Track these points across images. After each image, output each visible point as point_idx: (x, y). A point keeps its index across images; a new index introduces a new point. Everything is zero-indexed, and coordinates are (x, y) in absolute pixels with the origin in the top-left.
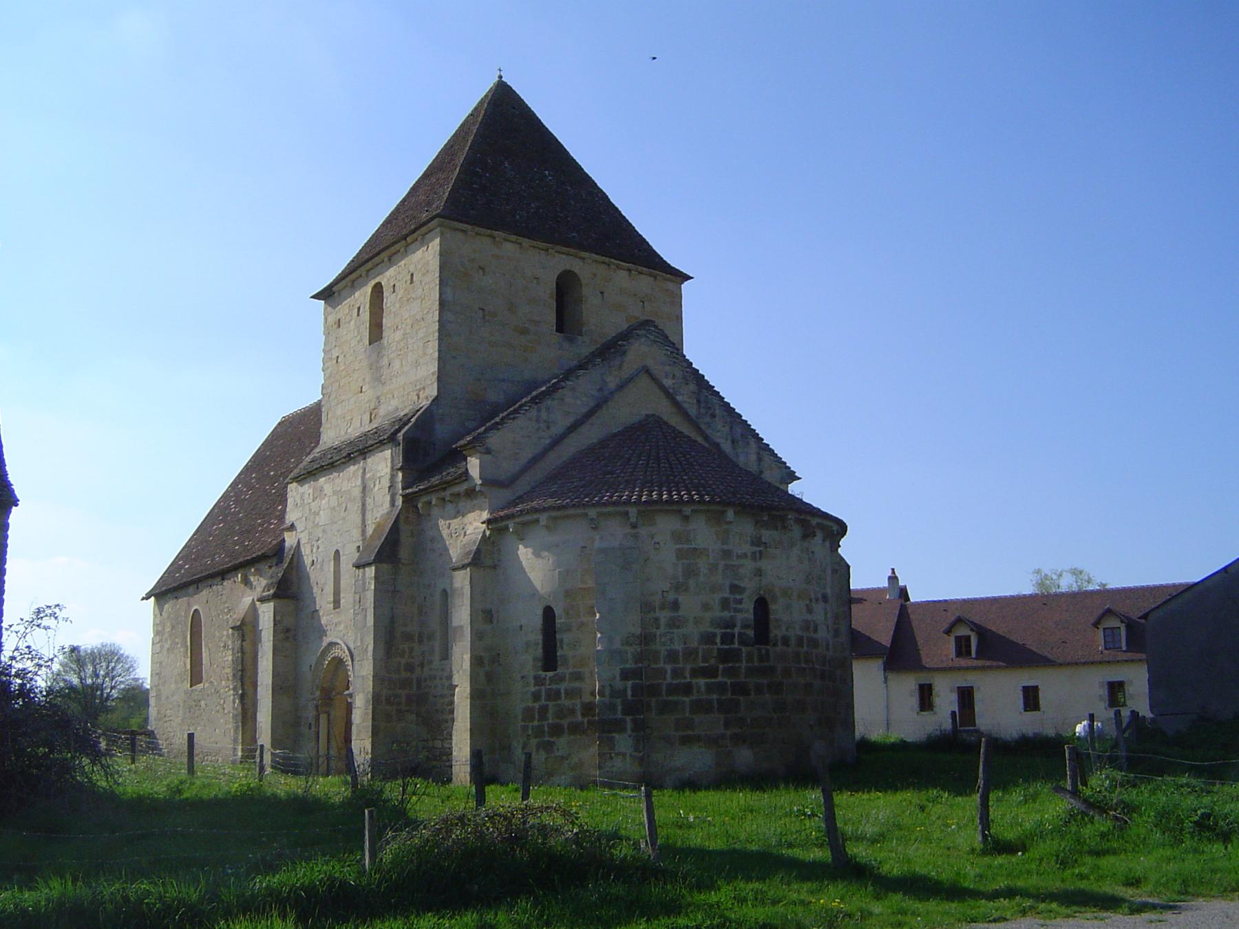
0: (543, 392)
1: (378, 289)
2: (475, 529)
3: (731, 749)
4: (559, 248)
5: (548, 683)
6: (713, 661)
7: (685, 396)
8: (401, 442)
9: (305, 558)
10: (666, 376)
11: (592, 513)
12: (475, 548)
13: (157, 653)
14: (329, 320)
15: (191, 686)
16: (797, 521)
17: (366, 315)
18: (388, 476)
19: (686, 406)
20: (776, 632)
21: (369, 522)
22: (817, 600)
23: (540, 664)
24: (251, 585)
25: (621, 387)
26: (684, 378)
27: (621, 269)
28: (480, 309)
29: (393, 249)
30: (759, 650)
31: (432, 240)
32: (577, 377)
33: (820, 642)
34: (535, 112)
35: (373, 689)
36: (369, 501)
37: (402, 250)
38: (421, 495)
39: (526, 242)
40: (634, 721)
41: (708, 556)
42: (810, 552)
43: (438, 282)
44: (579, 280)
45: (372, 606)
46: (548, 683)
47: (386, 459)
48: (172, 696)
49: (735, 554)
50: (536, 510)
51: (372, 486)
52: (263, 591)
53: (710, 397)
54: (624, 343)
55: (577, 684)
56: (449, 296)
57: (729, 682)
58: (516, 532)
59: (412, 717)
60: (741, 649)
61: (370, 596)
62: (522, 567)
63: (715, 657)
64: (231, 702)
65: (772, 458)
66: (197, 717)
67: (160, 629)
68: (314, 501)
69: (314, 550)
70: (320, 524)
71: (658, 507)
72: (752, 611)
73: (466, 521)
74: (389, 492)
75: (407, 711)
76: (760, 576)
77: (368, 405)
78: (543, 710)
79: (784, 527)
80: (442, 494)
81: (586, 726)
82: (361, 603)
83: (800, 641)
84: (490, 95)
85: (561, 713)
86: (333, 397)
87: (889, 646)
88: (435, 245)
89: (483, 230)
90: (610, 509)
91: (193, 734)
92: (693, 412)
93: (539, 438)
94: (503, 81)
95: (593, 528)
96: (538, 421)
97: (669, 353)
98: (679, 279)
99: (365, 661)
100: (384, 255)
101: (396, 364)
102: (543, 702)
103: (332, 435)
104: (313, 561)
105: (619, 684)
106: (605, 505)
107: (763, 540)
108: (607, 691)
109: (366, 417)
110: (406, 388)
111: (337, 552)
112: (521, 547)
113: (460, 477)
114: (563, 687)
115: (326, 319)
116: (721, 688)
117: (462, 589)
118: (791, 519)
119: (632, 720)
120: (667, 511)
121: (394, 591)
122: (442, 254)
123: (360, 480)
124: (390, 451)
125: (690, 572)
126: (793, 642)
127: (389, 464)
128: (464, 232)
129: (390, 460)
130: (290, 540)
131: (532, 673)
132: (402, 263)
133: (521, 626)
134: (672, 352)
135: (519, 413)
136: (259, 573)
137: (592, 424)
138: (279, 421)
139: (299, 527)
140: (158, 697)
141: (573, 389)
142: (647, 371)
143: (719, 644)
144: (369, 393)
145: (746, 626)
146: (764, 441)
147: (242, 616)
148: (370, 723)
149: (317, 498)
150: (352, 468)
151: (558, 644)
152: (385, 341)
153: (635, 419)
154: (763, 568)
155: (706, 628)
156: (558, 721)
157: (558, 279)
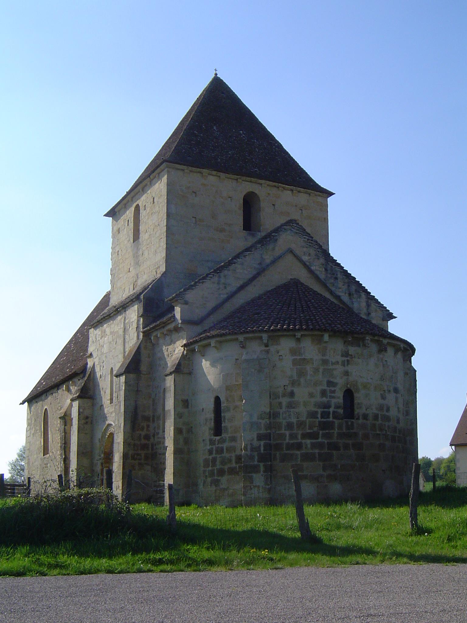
0: (222, 266)
1: (137, 207)
2: (179, 351)
3: (327, 484)
4: (244, 178)
5: (217, 443)
6: (315, 429)
7: (317, 267)
8: (142, 299)
9: (97, 373)
10: (305, 254)
11: (241, 338)
12: (178, 362)
13: (29, 437)
17: (132, 225)
18: (136, 321)
19: (318, 273)
23: (212, 432)
24: (71, 391)
25: (274, 262)
27: (286, 190)
30: (347, 422)
32: (245, 256)
33: (391, 417)
35: (123, 450)
36: (127, 337)
37: (148, 183)
38: (153, 332)
39: (222, 175)
42: (384, 361)
45: (123, 399)
46: (217, 443)
47: (135, 311)
48: (35, 462)
50: (209, 337)
51: (128, 328)
53: (334, 267)
54: (276, 234)
57: (326, 441)
59: (149, 468)
63: (317, 426)
65: (377, 305)
66: (46, 474)
67: (30, 422)
69: (101, 369)
70: (104, 353)
74: (136, 331)
75: (146, 464)
76: (348, 375)
77: (132, 279)
78: (214, 460)
79: (364, 345)
81: (238, 470)
82: (118, 398)
83: (376, 417)
88: (165, 179)
90: (251, 335)
92: (322, 276)
93: (220, 294)
95: (241, 347)
96: (218, 283)
97: (306, 240)
98: (325, 195)
99: (120, 433)
102: (214, 455)
104: (101, 375)
105: (256, 443)
106: (247, 332)
110: (150, 268)
112: (203, 360)
113: (171, 319)
114: (225, 446)
115: (113, 229)
116: (321, 446)
118: (368, 340)
119: (264, 465)
121: (138, 391)
122: (168, 185)
123: (123, 324)
125: (301, 373)
126: (370, 417)
127: (136, 314)
128: (183, 170)
129: (137, 311)
130: (90, 363)
132: (149, 192)
134: (308, 239)
135: (207, 279)
138: (105, 294)
139: (95, 355)
141: (242, 264)
142: (291, 251)
143: (320, 418)
144: (133, 272)
147: (65, 411)
148: (121, 471)
149: (102, 337)
150: (119, 318)
152: (140, 240)
153: (284, 282)
154: (349, 371)
157: (244, 196)
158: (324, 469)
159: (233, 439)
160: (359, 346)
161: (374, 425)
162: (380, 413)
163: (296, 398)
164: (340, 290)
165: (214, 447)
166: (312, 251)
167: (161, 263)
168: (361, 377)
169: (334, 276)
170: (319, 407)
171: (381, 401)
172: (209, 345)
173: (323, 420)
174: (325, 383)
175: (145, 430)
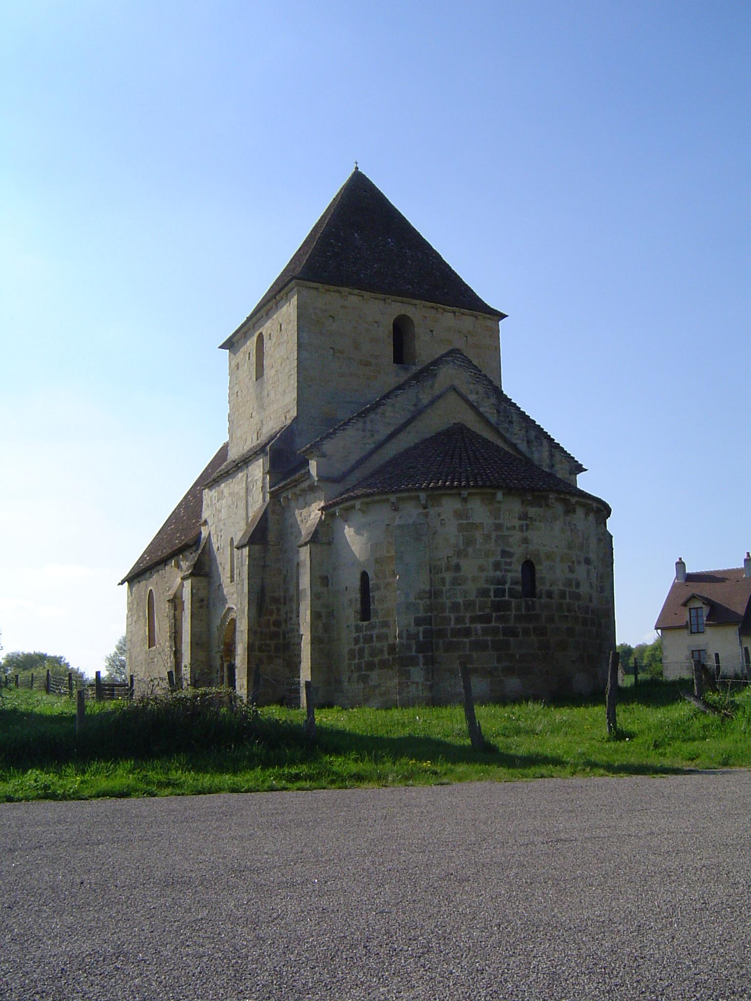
1: (261, 338)
3: (502, 678)
6: (488, 611)
7: (487, 408)
10: (471, 393)
11: (393, 498)
12: (314, 529)
14: (232, 364)
15: (149, 648)
16: (558, 499)
17: (254, 359)
18: (261, 479)
19: (488, 415)
20: (539, 588)
22: (579, 562)
24: (181, 568)
25: (432, 403)
26: (486, 393)
28: (330, 348)
30: (526, 602)
31: (292, 297)
32: (396, 396)
34: (384, 193)
36: (250, 499)
39: (367, 294)
43: (296, 329)
44: (412, 322)
49: (505, 527)
53: (508, 407)
54: (435, 368)
57: (501, 626)
58: (341, 516)
59: (279, 661)
60: (511, 602)
62: (347, 543)
65: (562, 454)
68: (218, 502)
69: (219, 539)
73: (311, 510)
78: (361, 651)
79: (547, 505)
83: (563, 595)
86: (235, 422)
87: (743, 615)
88: (294, 300)
89: (332, 288)
90: (405, 495)
92: (493, 420)
94: (358, 172)
95: (394, 510)
96: (364, 430)
98: (496, 318)
102: (362, 645)
105: (413, 629)
106: (401, 491)
107: (530, 516)
108: (405, 635)
109: (255, 437)
111: (232, 539)
112: (346, 527)
114: (375, 632)
115: (230, 364)
118: (552, 499)
119: (423, 657)
121: (264, 566)
124: (262, 460)
125: (469, 542)
127: (262, 470)
128: (317, 289)
130: (204, 534)
131: (354, 623)
132: (275, 317)
136: (186, 559)
137: (409, 432)
139: (210, 522)
141: (393, 406)
142: (454, 389)
144: (256, 418)
145: (516, 583)
146: (555, 441)
150: (240, 475)
151: (371, 599)
152: (265, 377)
155: (482, 584)
158: (499, 660)
168: (544, 546)
172: (353, 507)
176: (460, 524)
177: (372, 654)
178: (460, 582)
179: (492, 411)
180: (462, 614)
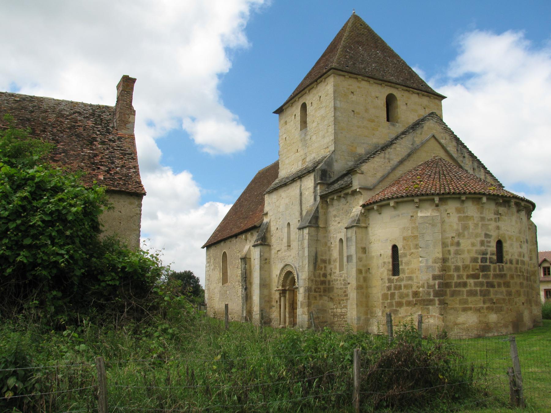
6: (477, 271)
7: (451, 148)
19: (452, 152)
20: (506, 257)
21: (304, 209)
29: (311, 87)
30: (499, 266)
32: (402, 138)
40: (439, 300)
41: (474, 220)
52: (255, 242)
55: (410, 282)
56: (338, 104)
61: (306, 242)
64: (240, 291)
67: (209, 260)
71: (448, 196)
72: (495, 246)
75: (324, 295)
76: (499, 229)
78: (393, 295)
80: (339, 194)
84: (350, 24)
85: (401, 296)
91: (228, 304)
92: (455, 156)
93: (386, 167)
96: (384, 158)
98: (440, 98)
100: (307, 90)
101: (314, 138)
102: (393, 291)
103: (284, 173)
105: (431, 282)
109: (300, 163)
114: (403, 283)
116: (481, 284)
117: (351, 237)
119: (438, 300)
120: (454, 198)
121: (317, 240)
125: (465, 228)
126: (514, 262)
130: (266, 220)
133: (381, 255)
139: (270, 214)
140: (209, 289)
144: (301, 152)
145: (493, 254)
152: (308, 129)
154: (500, 226)
156: (400, 300)
158: (484, 302)
159: (410, 278)
160: (505, 207)
161: (516, 268)
162: (519, 259)
163: (461, 247)
164: (467, 166)
165: (393, 284)
166: (448, 137)
167: (330, 144)
169: (463, 155)
170: (480, 254)
171: (520, 250)
173: (482, 264)
174: (483, 235)
175: (323, 269)
176: (459, 217)
177: (401, 296)
178: (460, 253)
179: (453, 150)
180: (461, 273)
